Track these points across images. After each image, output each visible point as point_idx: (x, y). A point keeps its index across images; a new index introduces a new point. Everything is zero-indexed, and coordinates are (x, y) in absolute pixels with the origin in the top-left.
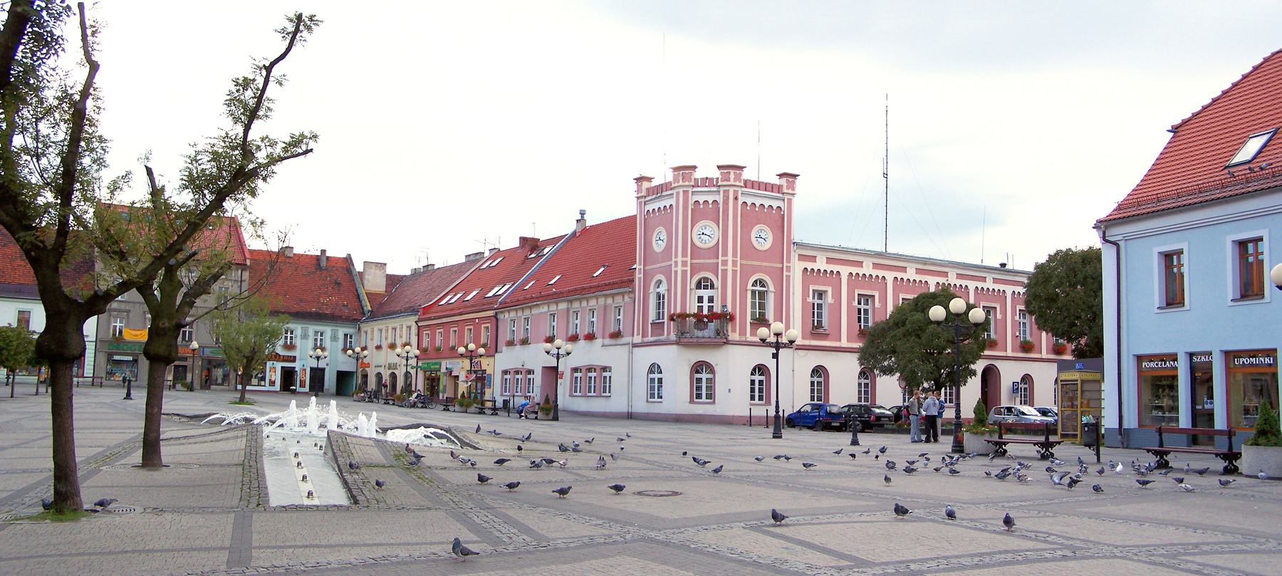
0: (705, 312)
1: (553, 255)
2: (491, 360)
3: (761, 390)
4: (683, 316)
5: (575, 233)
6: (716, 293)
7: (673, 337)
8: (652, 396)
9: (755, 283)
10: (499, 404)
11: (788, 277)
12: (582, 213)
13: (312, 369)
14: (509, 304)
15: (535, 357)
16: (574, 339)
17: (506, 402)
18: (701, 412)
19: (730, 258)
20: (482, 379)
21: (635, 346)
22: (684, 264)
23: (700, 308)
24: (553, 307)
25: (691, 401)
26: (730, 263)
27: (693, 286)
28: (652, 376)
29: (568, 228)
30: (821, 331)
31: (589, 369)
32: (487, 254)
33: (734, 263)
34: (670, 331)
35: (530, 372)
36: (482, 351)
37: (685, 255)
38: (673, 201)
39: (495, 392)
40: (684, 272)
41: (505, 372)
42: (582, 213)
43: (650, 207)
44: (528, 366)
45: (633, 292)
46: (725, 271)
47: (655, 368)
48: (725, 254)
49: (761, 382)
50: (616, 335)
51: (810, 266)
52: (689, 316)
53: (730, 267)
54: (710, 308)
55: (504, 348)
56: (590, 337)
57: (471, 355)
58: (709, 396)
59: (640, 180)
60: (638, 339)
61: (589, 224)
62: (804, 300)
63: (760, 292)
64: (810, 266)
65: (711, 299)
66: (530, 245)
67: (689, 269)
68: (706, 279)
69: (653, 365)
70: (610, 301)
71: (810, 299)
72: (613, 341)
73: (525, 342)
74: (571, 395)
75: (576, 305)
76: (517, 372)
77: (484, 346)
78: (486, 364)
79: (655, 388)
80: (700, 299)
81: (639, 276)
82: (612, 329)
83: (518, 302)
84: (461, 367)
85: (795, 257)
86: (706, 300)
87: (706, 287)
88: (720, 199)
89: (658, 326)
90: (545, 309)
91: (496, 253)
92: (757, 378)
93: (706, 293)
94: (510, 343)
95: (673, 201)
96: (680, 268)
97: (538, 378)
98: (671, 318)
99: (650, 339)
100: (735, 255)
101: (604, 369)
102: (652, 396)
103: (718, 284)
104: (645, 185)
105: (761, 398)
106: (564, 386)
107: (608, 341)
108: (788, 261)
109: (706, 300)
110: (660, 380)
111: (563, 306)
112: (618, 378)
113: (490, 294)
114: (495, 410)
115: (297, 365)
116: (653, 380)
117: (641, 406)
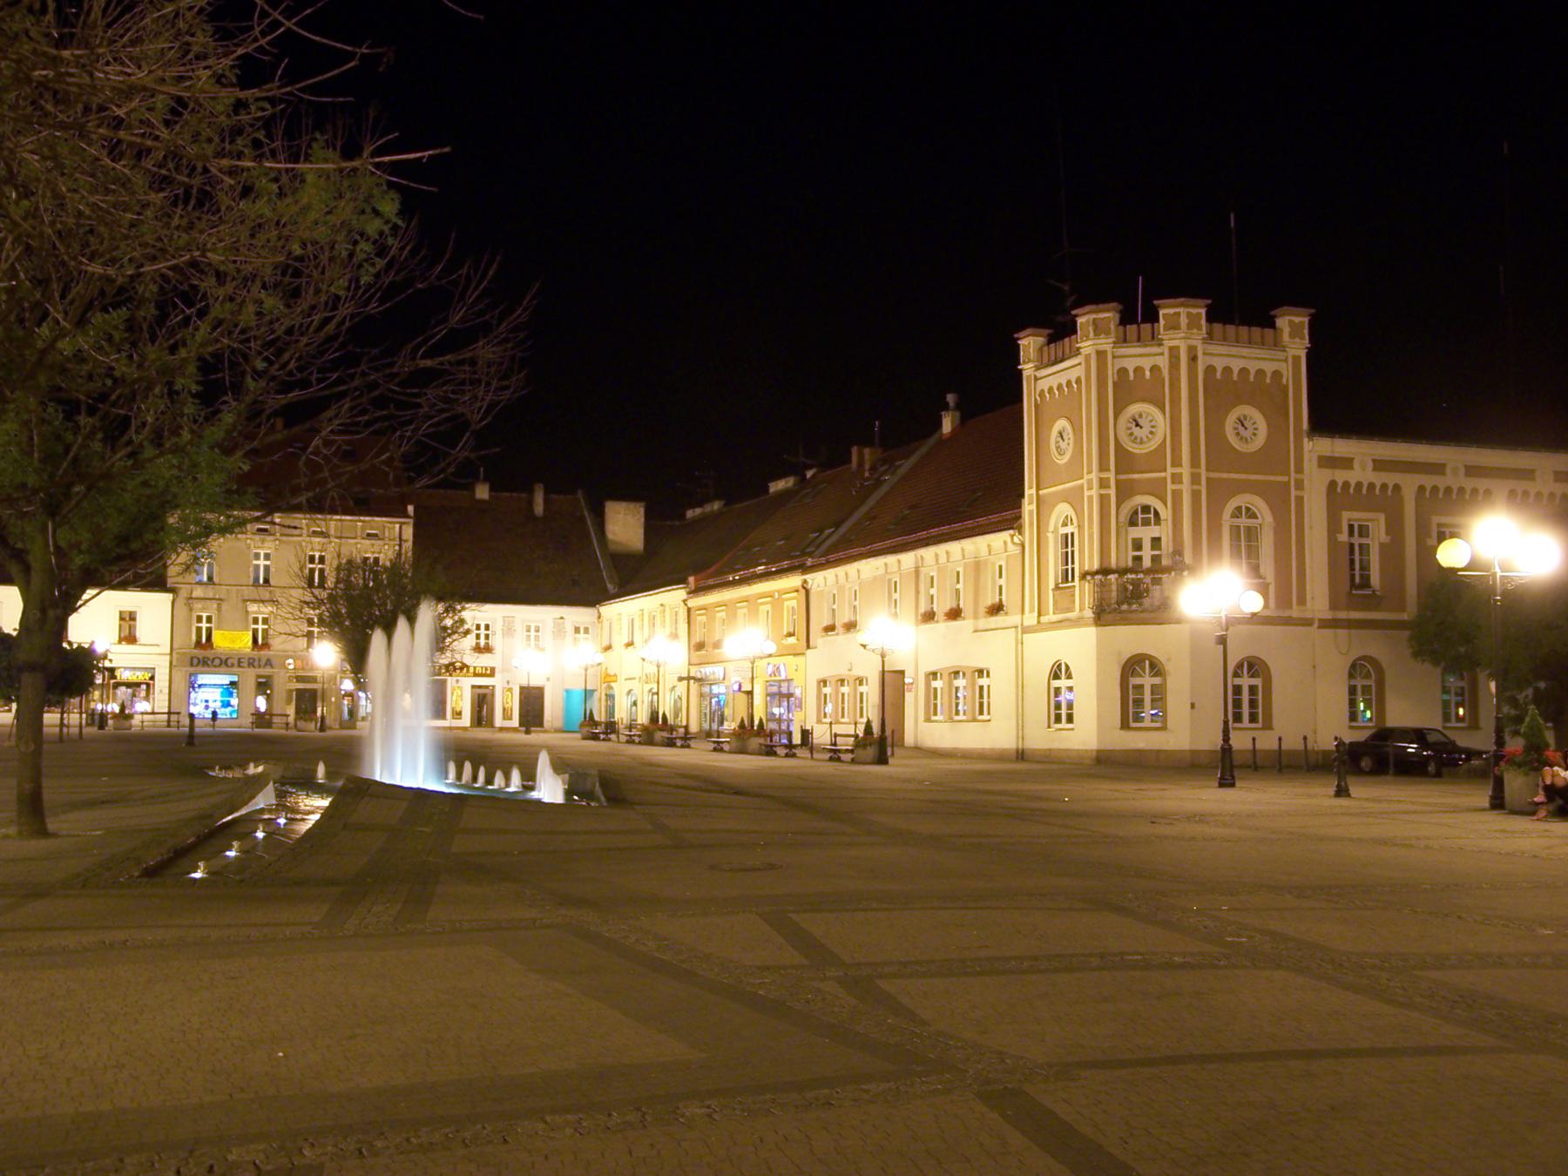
0: (1147, 563)
2: (800, 659)
3: (1253, 704)
6: (1164, 531)
8: (1058, 719)
9: (1237, 512)
11: (1300, 500)
13: (522, 689)
18: (1141, 745)
19: (1185, 471)
21: (1026, 630)
23: (1138, 559)
25: (1125, 725)
26: (1186, 479)
27: (1124, 517)
28: (1056, 683)
30: (208, 653)
33: (1195, 479)
35: (860, 681)
44: (857, 672)
46: (1177, 495)
48: (1177, 462)
49: (1253, 689)
50: (996, 609)
51: (1341, 476)
53: (1186, 487)
54: (1155, 559)
58: (1070, 719)
62: (1332, 542)
63: (1248, 529)
64: (1341, 476)
65: (1156, 541)
67: (1112, 492)
68: (1146, 509)
71: (1343, 537)
74: (928, 720)
80: (1138, 545)
82: (990, 599)
85: (1310, 464)
86: (1147, 544)
87: (1146, 523)
88: (1163, 362)
92: (1245, 682)
93: (1145, 533)
94: (830, 629)
100: (1195, 462)
102: (1058, 719)
103: (1165, 513)
105: (1253, 718)
106: (913, 705)
108: (1299, 470)
109: (1147, 544)
112: (1000, 689)
115: (496, 682)
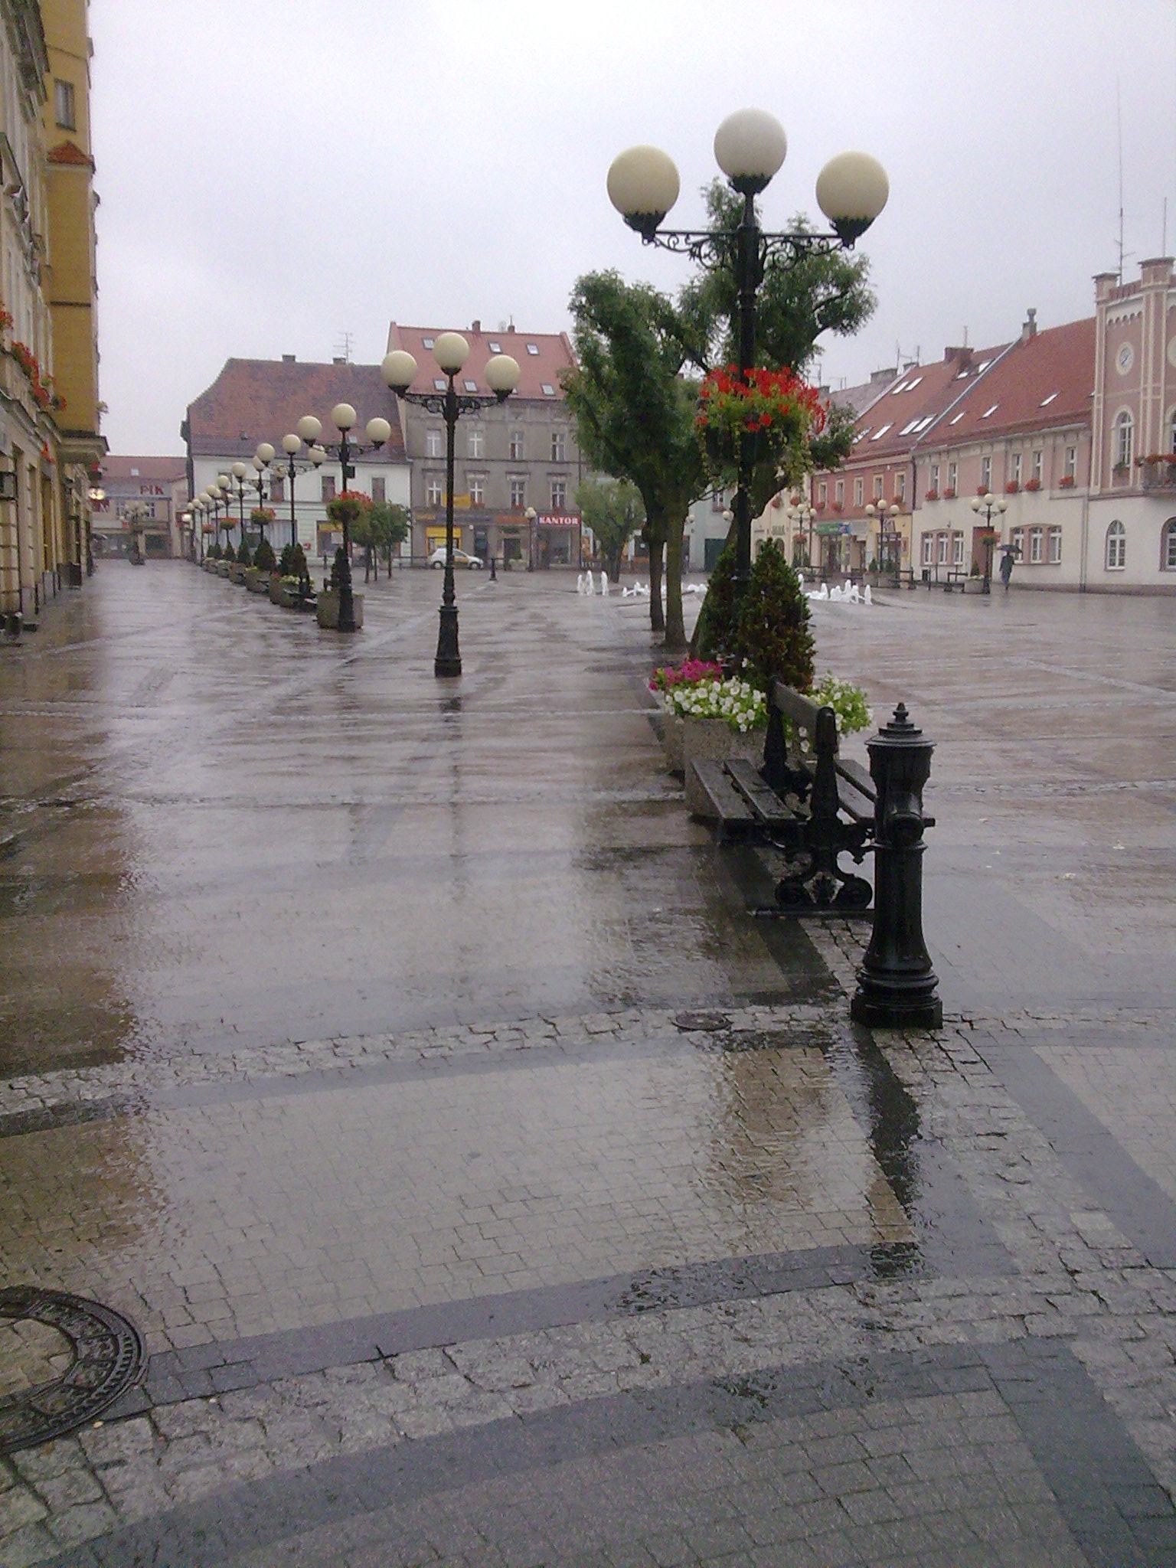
1: (988, 374)
4: (1154, 459)
5: (1019, 343)
7: (1140, 488)
10: (918, 576)
12: (1032, 313)
14: (928, 443)
15: (962, 515)
16: (1012, 489)
17: (925, 573)
20: (893, 543)
22: (1156, 391)
24: (987, 450)
25: (1162, 568)
28: (1112, 537)
29: (1013, 334)
31: (1034, 530)
32: (901, 371)
34: (1136, 478)
35: (957, 534)
36: (895, 508)
37: (1156, 379)
38: (1135, 309)
39: (913, 562)
40: (1156, 403)
41: (926, 535)
42: (1032, 313)
43: (1113, 315)
44: (955, 527)
45: (1090, 428)
47: (1115, 527)
52: (1160, 459)
55: (925, 504)
56: (1034, 487)
57: (882, 516)
59: (1100, 279)
60: (1095, 490)
61: (1040, 329)
66: (961, 358)
67: (1162, 397)
69: (1115, 523)
70: (1060, 440)
72: (1065, 493)
73: (950, 495)
75: (1017, 447)
76: (941, 535)
77: (898, 501)
78: (899, 524)
79: (1116, 552)
81: (1097, 407)
83: (948, 441)
84: (869, 532)
89: (1121, 470)
90: (977, 451)
91: (914, 369)
94: (932, 497)
95: (1135, 309)
96: (1149, 397)
97: (967, 542)
98: (1137, 463)
99: (1111, 488)
101: (1053, 529)
104: (1107, 285)
107: (1058, 493)
110: (1122, 543)
111: (1000, 448)
113: (906, 431)
114: (912, 584)
116: (1113, 542)
117: (1097, 575)
